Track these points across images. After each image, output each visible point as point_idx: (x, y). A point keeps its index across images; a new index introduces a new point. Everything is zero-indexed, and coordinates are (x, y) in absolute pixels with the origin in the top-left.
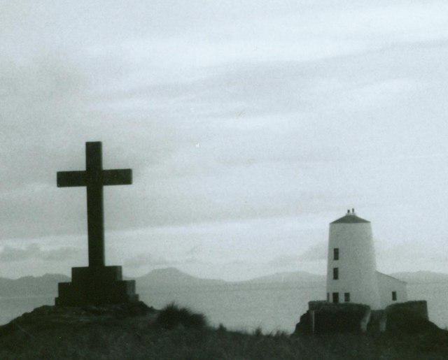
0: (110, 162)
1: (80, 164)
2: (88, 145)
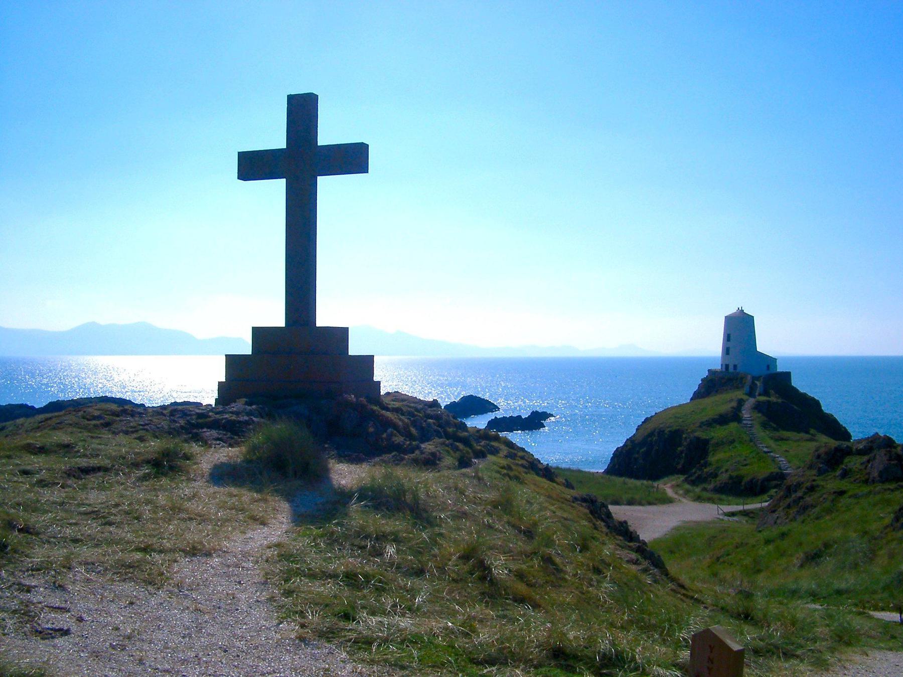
0: (273, 136)
1: (330, 132)
2: (291, 99)
